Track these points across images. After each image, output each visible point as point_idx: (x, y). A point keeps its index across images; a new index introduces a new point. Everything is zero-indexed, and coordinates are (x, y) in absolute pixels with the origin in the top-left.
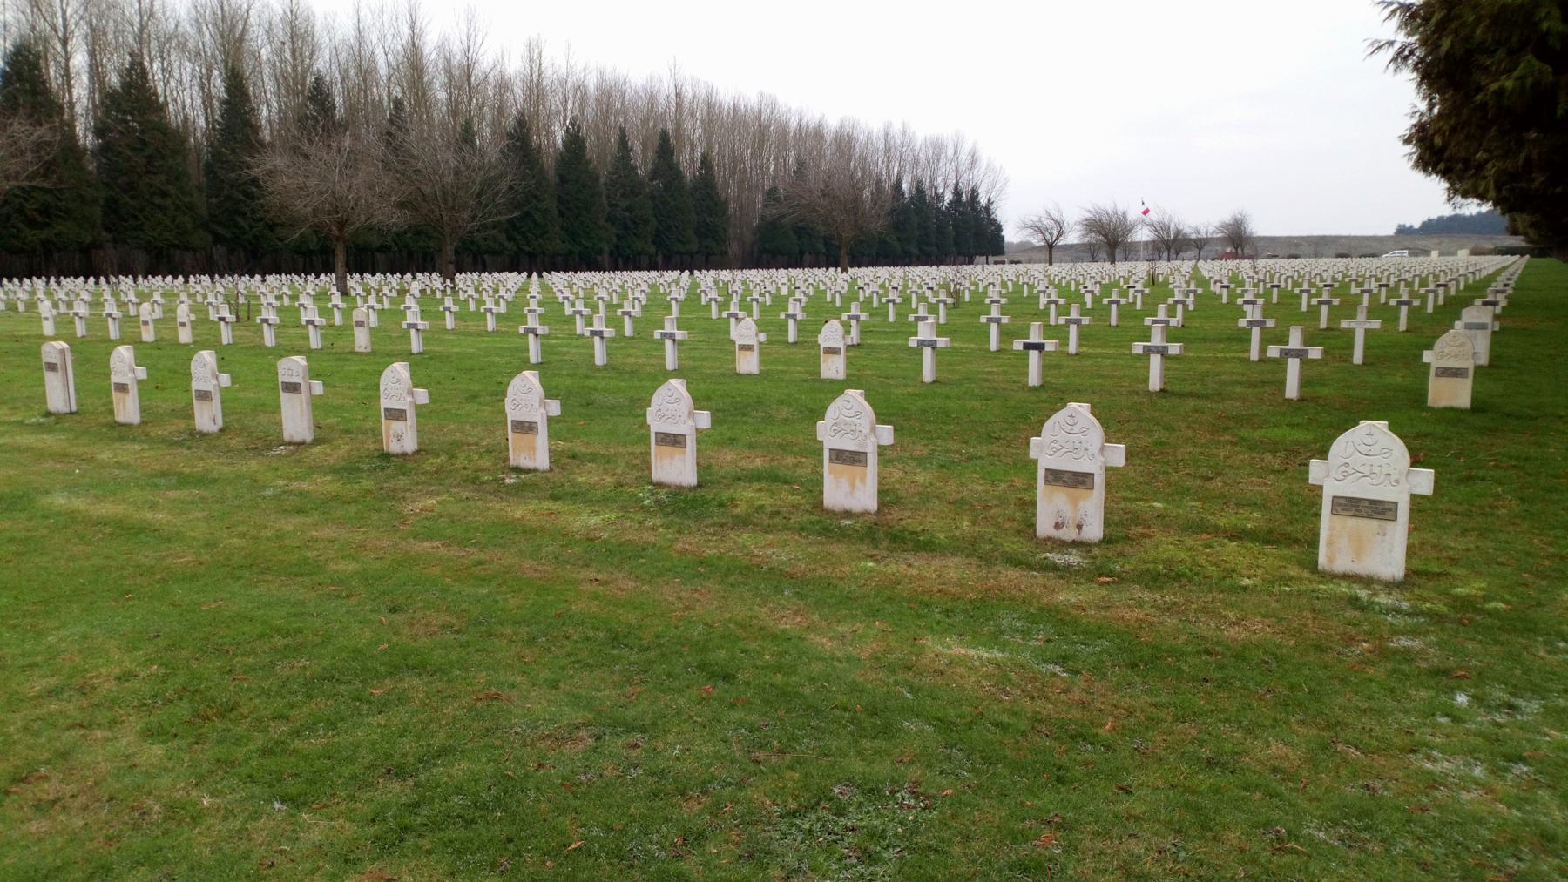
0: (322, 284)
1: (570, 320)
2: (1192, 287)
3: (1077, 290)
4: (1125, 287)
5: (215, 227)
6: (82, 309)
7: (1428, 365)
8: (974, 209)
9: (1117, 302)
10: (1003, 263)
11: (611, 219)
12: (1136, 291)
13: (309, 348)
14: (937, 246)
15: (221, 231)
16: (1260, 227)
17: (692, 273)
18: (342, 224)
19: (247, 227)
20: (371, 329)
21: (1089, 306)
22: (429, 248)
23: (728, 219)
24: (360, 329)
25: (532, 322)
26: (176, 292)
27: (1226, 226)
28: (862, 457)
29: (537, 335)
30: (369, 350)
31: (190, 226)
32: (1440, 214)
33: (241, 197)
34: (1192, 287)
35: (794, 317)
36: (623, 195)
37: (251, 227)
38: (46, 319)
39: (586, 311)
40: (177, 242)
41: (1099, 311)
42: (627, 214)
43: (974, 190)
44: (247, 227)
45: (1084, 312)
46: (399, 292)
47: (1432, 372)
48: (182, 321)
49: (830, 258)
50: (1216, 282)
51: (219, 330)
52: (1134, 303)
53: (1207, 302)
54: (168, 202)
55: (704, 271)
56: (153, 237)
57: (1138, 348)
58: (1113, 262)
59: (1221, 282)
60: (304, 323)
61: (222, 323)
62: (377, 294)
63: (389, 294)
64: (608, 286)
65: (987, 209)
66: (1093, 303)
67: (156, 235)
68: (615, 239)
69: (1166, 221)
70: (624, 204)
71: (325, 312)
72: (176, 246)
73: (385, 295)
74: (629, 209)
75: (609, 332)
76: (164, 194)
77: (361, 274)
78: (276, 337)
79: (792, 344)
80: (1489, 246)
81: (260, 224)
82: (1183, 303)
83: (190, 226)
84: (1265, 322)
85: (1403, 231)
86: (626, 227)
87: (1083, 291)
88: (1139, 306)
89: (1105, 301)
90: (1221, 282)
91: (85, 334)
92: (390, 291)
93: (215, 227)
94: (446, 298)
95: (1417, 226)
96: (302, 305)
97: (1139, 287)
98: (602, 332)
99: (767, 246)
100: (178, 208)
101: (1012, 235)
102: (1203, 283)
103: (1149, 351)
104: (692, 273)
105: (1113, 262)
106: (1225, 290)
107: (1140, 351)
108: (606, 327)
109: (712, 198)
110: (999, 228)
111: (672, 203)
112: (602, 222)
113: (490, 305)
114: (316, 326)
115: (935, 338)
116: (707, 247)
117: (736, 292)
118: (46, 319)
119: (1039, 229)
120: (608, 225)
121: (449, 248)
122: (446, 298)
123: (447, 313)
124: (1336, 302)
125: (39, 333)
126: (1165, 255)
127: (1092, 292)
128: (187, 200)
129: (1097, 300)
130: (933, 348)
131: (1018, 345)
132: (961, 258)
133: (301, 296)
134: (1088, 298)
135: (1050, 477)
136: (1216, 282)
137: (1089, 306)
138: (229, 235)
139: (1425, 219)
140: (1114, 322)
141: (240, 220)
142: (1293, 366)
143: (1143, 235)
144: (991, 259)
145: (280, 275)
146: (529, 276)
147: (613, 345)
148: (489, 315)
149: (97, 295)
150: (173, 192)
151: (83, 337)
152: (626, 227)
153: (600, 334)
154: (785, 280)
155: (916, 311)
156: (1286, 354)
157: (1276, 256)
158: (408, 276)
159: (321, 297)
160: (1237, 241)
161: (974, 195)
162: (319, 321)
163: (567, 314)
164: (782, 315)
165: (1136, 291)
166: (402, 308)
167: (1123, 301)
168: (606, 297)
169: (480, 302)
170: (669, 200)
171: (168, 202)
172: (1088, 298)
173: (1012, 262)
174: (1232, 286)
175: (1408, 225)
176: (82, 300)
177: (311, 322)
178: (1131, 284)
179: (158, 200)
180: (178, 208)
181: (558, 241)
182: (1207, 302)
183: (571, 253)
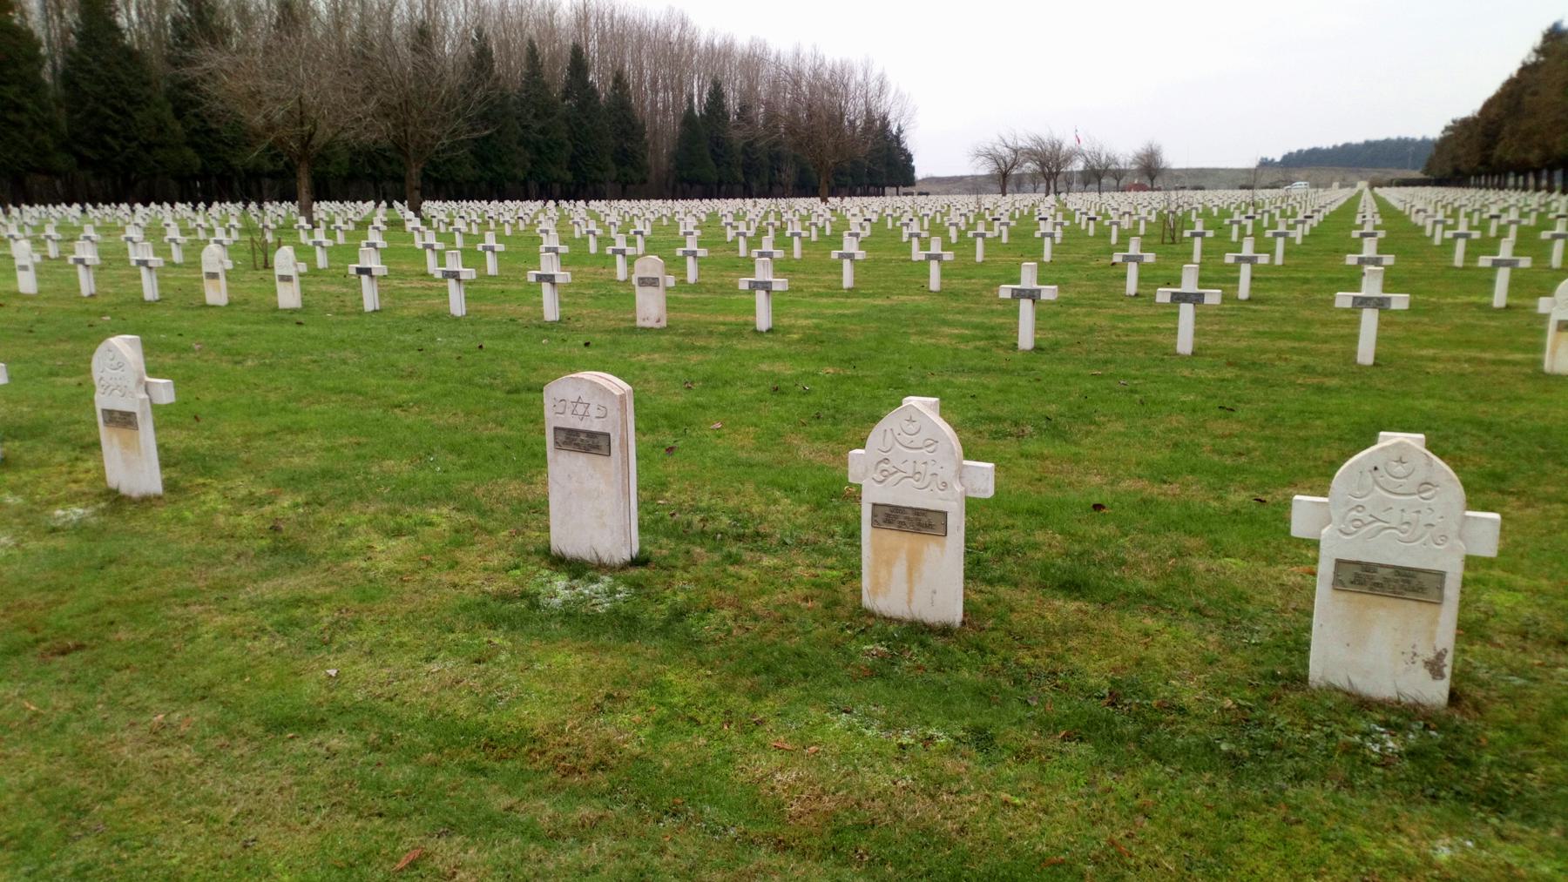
0: (152, 213)
1: (420, 256)
2: (1059, 219)
3: (942, 223)
4: (990, 219)
5: (77, 147)
6: (87, 253)
7: (1545, 318)
8: (886, 137)
9: (983, 236)
10: (912, 194)
11: (524, 142)
12: (1002, 224)
13: (142, 300)
14: (852, 176)
15: (88, 153)
16: (1175, 158)
17: (390, 206)
18: (306, 141)
19: (118, 148)
20: (667, 289)
21: (954, 241)
22: (329, 173)
23: (646, 144)
24: (649, 289)
25: (549, 265)
26: (120, 224)
27: (1140, 157)
28: (603, 443)
29: (150, 268)
30: (664, 324)
31: (51, 146)
32: (1299, 148)
33: (109, 112)
34: (1059, 219)
35: (850, 256)
36: (536, 116)
37: (123, 148)
38: (24, 268)
39: (438, 246)
40: (35, 165)
41: (965, 244)
42: (541, 137)
43: (885, 118)
44: (118, 148)
45: (947, 245)
46: (357, 224)
47: (1552, 327)
48: (285, 273)
49: (805, 188)
50: (1418, 211)
51: (76, 274)
52: (1000, 236)
53: (1073, 235)
54: (24, 118)
55: (25, 207)
56: (8, 159)
57: (1344, 299)
58: (1004, 194)
59: (1425, 211)
60: (133, 264)
61: (365, 278)
62: (328, 228)
63: (344, 227)
64: (466, 216)
65: (897, 137)
66: (959, 237)
67: (10, 155)
68: (529, 165)
69: (1097, 150)
70: (537, 125)
71: (162, 250)
72: (37, 171)
73: (339, 228)
74: (543, 131)
75: (468, 274)
76: (19, 109)
77: (556, 201)
78: (160, 287)
79: (1499, 310)
80: (1389, 177)
81: (135, 144)
82: (1052, 236)
83: (51, 146)
84: (1517, 262)
85: (1265, 164)
86: (539, 151)
87: (947, 224)
88: (1004, 240)
89: (970, 234)
90: (1425, 211)
91: (93, 291)
92: (345, 223)
93: (77, 147)
94: (488, 234)
95: (1278, 159)
96: (130, 239)
97: (1004, 219)
98: (553, 276)
99: (685, 174)
100: (35, 124)
101: (920, 172)
102: (1069, 215)
103: (793, 235)
104: (390, 206)
105: (1004, 194)
106: (1250, 221)
107: (1349, 305)
108: (464, 266)
109: (629, 122)
110: (909, 158)
111: (589, 126)
112: (514, 146)
113: (621, 244)
114: (150, 268)
115: (770, 279)
116: (625, 175)
117: (614, 224)
118: (24, 268)
119: (995, 158)
120: (521, 149)
121: (414, 171)
122: (488, 234)
123: (489, 254)
124: (1210, 234)
125: (12, 288)
126: (1043, 186)
127: (956, 225)
128: (46, 116)
129: (961, 234)
130: (768, 292)
131: (1163, 295)
132: (872, 189)
133: (127, 227)
134: (953, 232)
135: (562, 437)
136: (1418, 211)
137: (954, 241)
138: (95, 157)
139: (1286, 153)
140: (979, 258)
141: (108, 139)
142: (1369, 318)
143: (1078, 165)
144: (902, 189)
145: (46, 206)
146: (377, 206)
147: (474, 293)
148: (489, 254)
149: (396, 224)
150: (30, 105)
151: (92, 296)
152: (539, 151)
153: (455, 275)
154: (856, 210)
155: (1237, 247)
156: (1361, 303)
157: (1183, 188)
158: (253, 206)
159: (154, 233)
160: (1150, 172)
161: (885, 124)
162: (156, 261)
163: (915, 258)
164: (834, 254)
165: (1002, 224)
166: (609, 252)
167: (989, 235)
168: (464, 229)
169: (604, 241)
170: (585, 122)
171: (24, 118)
172: (953, 232)
173: (920, 194)
174: (1099, 218)
175: (1270, 158)
176: (88, 238)
177: (144, 263)
178: (996, 216)
179: (11, 116)
180: (35, 124)
181: (468, 166)
182: (1073, 235)
183: (481, 178)
